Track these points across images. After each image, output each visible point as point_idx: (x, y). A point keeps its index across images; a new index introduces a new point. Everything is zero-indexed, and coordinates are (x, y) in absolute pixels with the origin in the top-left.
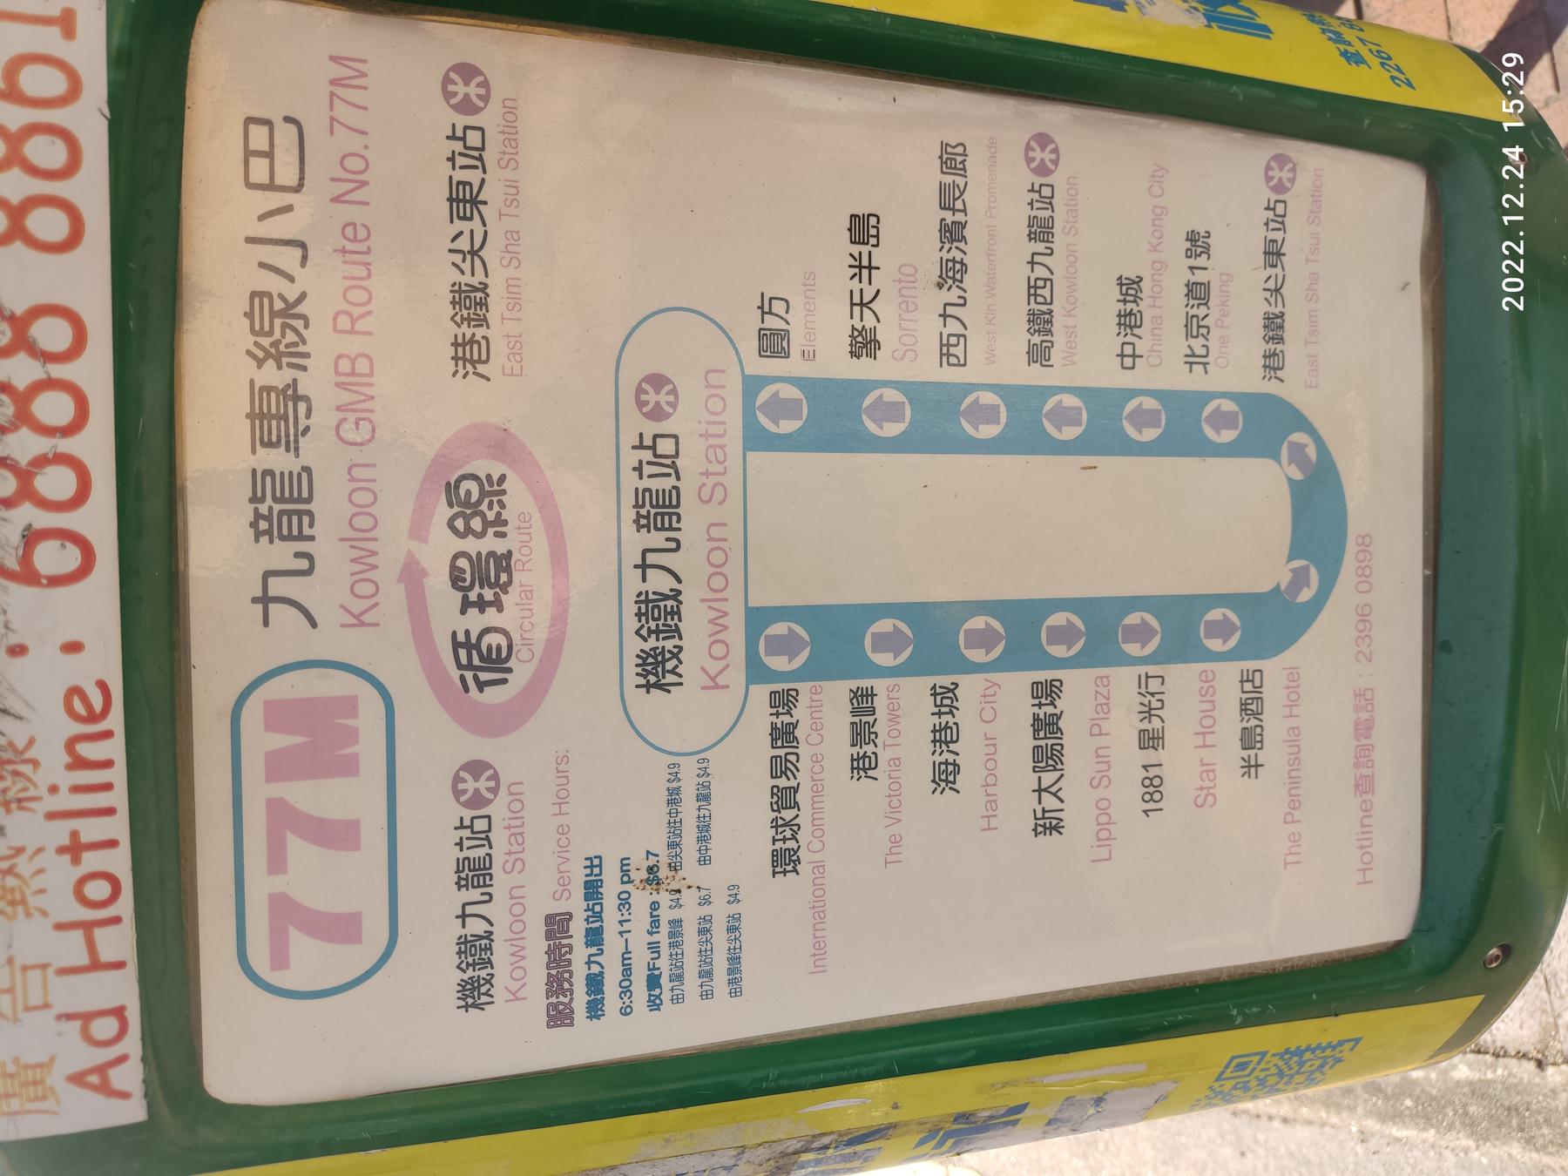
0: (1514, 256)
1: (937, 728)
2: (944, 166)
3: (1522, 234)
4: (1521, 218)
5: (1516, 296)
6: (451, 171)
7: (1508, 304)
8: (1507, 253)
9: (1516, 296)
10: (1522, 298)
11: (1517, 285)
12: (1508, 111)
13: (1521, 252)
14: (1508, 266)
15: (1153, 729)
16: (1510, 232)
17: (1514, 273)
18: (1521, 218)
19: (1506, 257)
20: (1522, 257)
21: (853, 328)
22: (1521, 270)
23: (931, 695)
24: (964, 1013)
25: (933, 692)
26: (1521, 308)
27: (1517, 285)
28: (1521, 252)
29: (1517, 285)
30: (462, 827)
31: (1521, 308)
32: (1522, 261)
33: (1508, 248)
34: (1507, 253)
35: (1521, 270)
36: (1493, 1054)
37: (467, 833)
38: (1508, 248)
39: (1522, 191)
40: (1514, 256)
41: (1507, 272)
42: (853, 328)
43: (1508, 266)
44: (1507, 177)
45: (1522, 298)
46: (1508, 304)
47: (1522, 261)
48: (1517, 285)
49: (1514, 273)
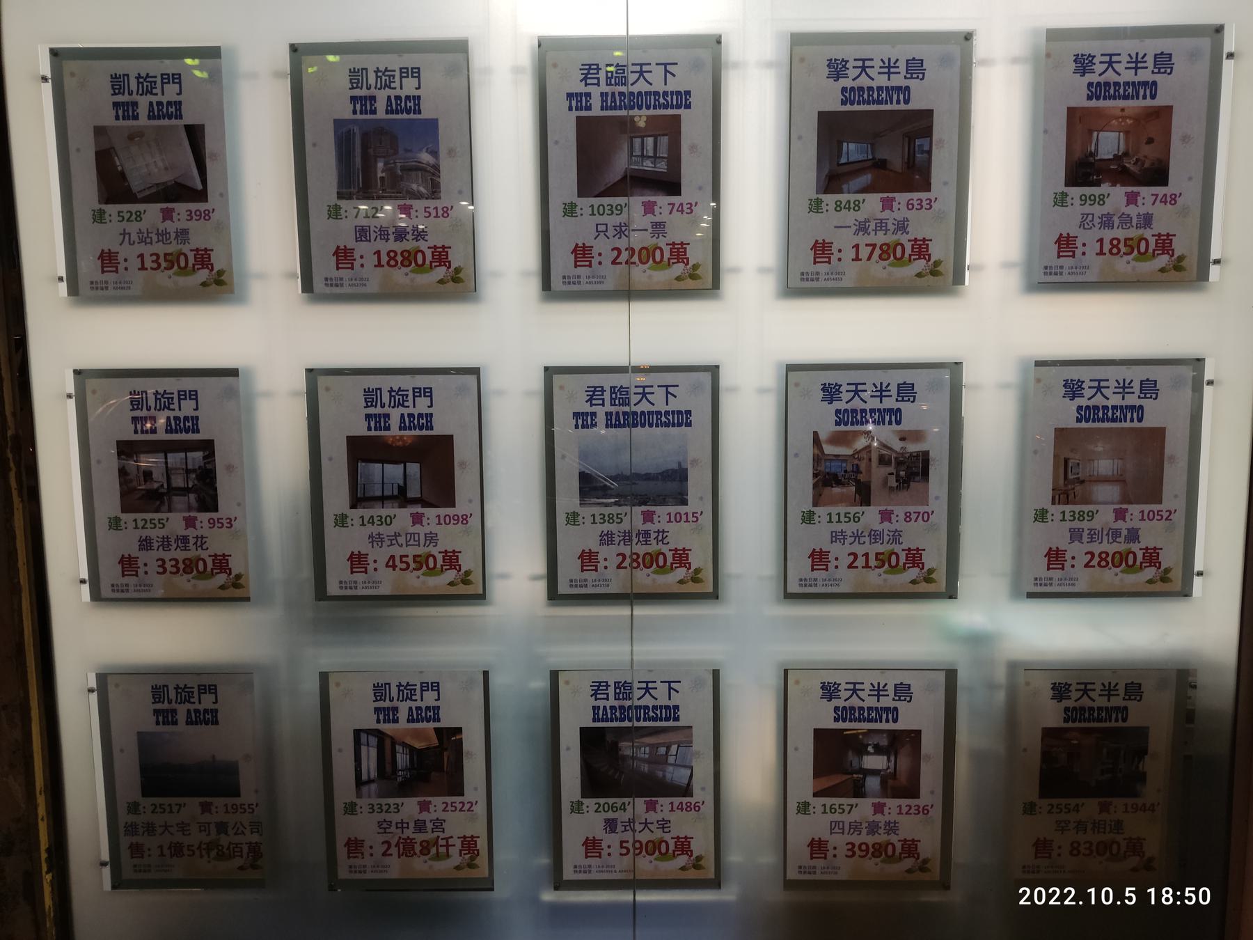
0: (1063, 897)
1: (381, 536)
2: (234, 846)
3: (1081, 903)
4: (1153, 903)
5: (1031, 898)
6: (664, 86)
7: (1025, 892)
8: (1065, 891)
9: (1031, 898)
10: (1029, 903)
11: (1040, 899)
12: (1187, 892)
13: (1066, 902)
14: (1055, 892)
15: (250, 826)
16: (1082, 895)
17: (1049, 897)
18: (1153, 903)
19: (1062, 891)
20: (1062, 903)
21: (1094, 57)
22: (1051, 902)
23: (620, 223)
24: (200, 603)
25: (623, 224)
26: (1022, 902)
27: (1040, 900)
28: (1066, 902)
29: (1040, 900)
30: (148, 233)
31: (1022, 902)
32: (1059, 903)
33: (1070, 892)
34: (1065, 891)
35: (1051, 902)
36: (620, 871)
37: (145, 235)
38: (1070, 892)
39: (1077, 903)
40: (1063, 897)
41: (1050, 891)
42: (1094, 57)
43: (1055, 892)
44: (1021, 891)
45: (1029, 903)
46: (1025, 892)
47: (1059, 903)
48: (1040, 899)
49: (1049, 897)
